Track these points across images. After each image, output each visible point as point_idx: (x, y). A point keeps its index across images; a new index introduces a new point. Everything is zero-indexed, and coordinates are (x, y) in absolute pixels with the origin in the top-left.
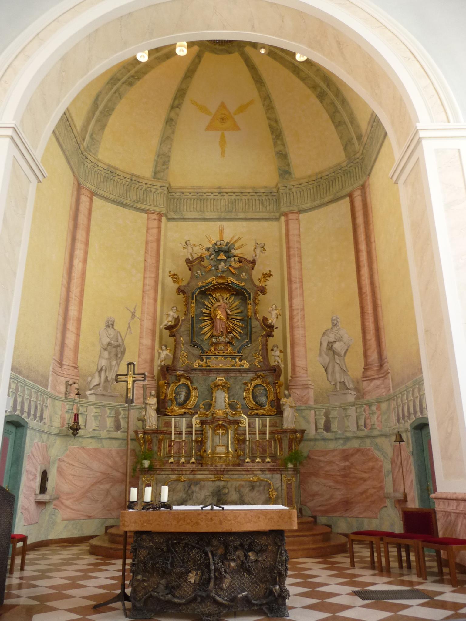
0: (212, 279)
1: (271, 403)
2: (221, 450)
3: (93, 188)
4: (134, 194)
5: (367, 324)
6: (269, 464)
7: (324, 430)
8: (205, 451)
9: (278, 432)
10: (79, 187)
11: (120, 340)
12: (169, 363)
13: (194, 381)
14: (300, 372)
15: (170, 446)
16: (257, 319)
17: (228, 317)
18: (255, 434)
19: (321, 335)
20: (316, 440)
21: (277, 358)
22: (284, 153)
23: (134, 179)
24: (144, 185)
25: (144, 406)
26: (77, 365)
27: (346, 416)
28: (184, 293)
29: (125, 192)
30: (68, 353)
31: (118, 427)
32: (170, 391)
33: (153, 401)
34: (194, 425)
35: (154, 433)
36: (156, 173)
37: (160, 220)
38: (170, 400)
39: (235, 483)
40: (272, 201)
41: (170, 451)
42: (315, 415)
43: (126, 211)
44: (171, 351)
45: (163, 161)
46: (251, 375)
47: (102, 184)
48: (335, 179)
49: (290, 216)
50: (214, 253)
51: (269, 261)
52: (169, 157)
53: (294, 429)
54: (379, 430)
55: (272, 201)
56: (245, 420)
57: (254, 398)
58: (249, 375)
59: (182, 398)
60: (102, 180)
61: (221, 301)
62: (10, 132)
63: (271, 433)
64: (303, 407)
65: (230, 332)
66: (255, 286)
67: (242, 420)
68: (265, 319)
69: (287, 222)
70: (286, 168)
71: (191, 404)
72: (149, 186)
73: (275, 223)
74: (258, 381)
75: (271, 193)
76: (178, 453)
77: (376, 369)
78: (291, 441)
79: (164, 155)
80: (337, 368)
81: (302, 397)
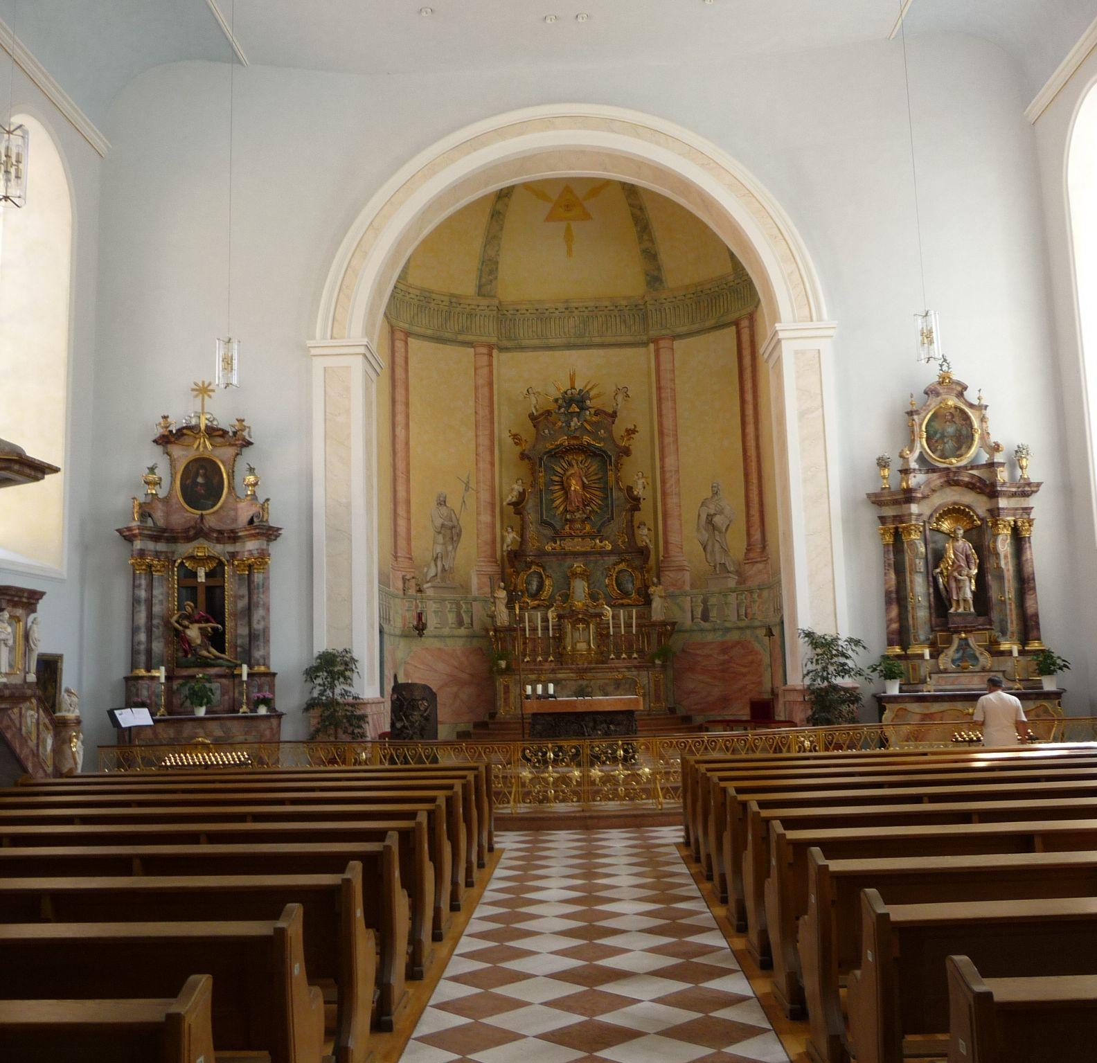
0: (563, 440)
1: (638, 592)
2: (582, 646)
3: (407, 326)
4: (456, 322)
5: (751, 496)
6: (636, 661)
7: (702, 619)
8: (564, 648)
9: (646, 625)
10: (393, 331)
11: (454, 519)
12: (515, 547)
13: (547, 568)
14: (674, 551)
15: (525, 643)
16: (620, 489)
17: (584, 487)
18: (620, 627)
19: (700, 505)
20: (692, 631)
21: (644, 537)
22: (653, 252)
23: (455, 300)
24: (467, 306)
25: (492, 600)
26: (411, 554)
27: (726, 604)
28: (529, 458)
29: (444, 322)
30: (402, 543)
31: (460, 623)
32: (520, 581)
33: (502, 594)
34: (550, 620)
35: (507, 630)
36: (480, 287)
37: (490, 355)
38: (521, 591)
39: (598, 682)
40: (637, 319)
41: (525, 649)
42: (692, 601)
43: (448, 347)
44: (517, 532)
45: (489, 269)
46: (613, 559)
47: (416, 317)
48: (719, 296)
49: (662, 344)
50: (564, 404)
51: (635, 414)
52: (498, 262)
53: (664, 621)
54: (760, 621)
55: (637, 319)
56: (608, 611)
57: (618, 585)
58: (612, 558)
59: (534, 586)
60: (415, 312)
61: (575, 466)
62: (362, 350)
63: (638, 625)
64: (677, 592)
65: (588, 505)
66: (617, 446)
67: (605, 612)
68: (630, 489)
69: (657, 352)
70: (656, 273)
71: (545, 594)
72: (473, 307)
73: (642, 350)
74: (622, 566)
75: (636, 306)
76: (534, 650)
77: (759, 550)
78: (660, 635)
79: (489, 260)
80: (717, 546)
81: (676, 581)
